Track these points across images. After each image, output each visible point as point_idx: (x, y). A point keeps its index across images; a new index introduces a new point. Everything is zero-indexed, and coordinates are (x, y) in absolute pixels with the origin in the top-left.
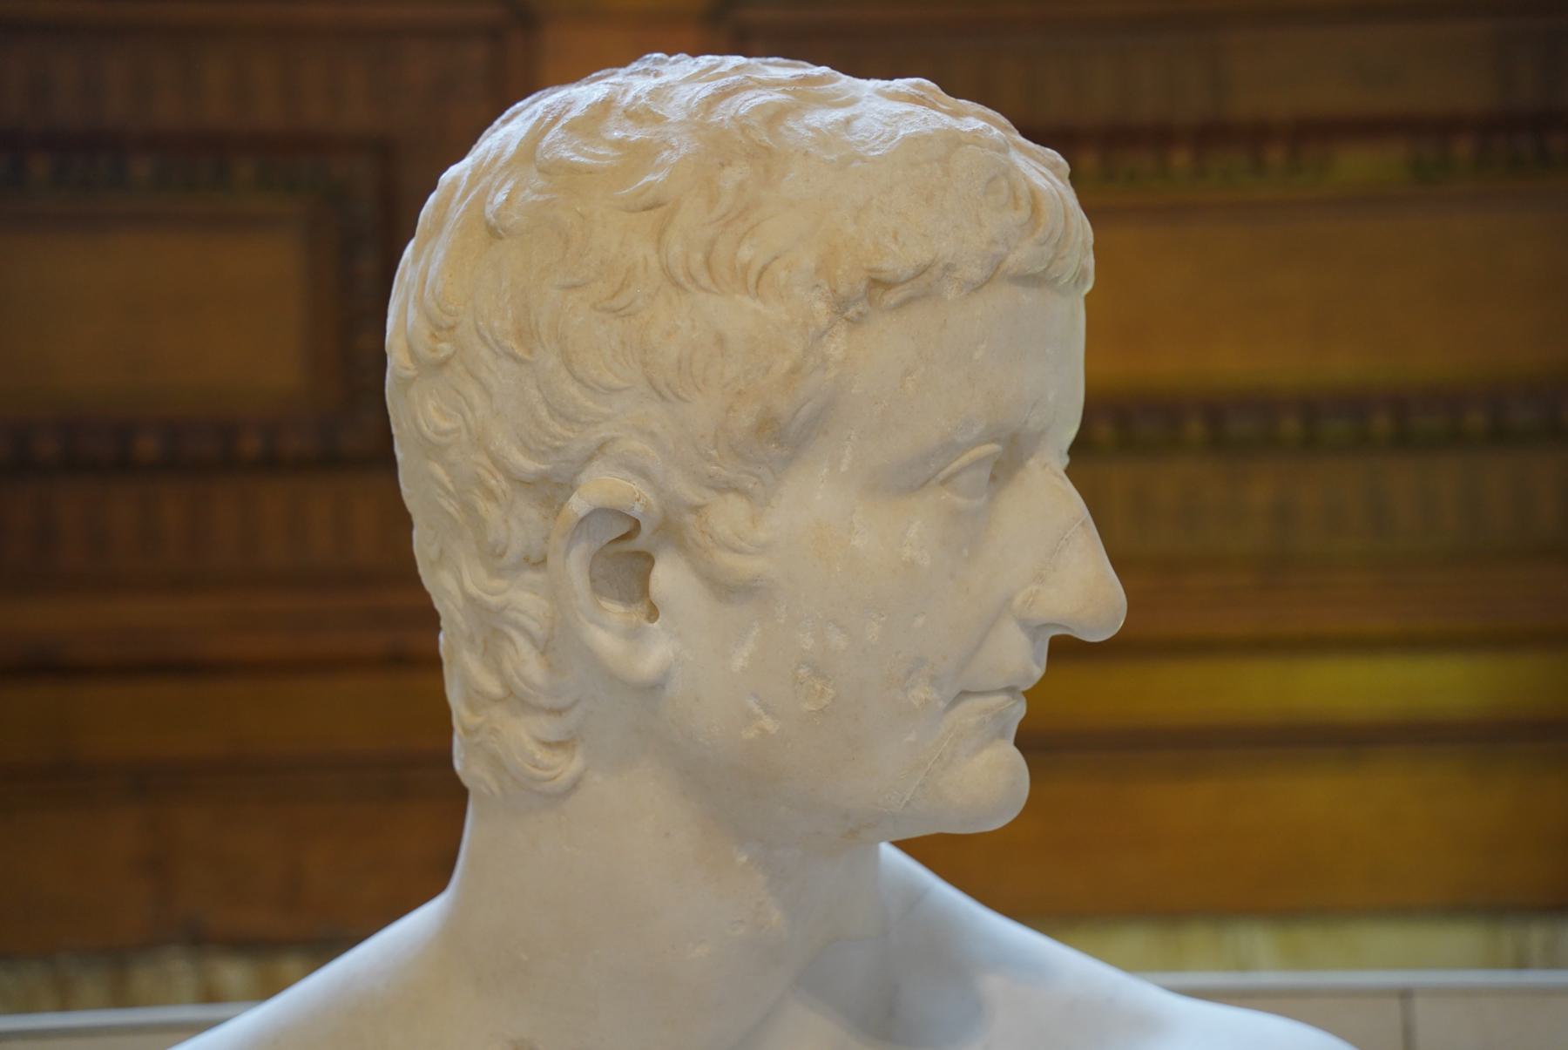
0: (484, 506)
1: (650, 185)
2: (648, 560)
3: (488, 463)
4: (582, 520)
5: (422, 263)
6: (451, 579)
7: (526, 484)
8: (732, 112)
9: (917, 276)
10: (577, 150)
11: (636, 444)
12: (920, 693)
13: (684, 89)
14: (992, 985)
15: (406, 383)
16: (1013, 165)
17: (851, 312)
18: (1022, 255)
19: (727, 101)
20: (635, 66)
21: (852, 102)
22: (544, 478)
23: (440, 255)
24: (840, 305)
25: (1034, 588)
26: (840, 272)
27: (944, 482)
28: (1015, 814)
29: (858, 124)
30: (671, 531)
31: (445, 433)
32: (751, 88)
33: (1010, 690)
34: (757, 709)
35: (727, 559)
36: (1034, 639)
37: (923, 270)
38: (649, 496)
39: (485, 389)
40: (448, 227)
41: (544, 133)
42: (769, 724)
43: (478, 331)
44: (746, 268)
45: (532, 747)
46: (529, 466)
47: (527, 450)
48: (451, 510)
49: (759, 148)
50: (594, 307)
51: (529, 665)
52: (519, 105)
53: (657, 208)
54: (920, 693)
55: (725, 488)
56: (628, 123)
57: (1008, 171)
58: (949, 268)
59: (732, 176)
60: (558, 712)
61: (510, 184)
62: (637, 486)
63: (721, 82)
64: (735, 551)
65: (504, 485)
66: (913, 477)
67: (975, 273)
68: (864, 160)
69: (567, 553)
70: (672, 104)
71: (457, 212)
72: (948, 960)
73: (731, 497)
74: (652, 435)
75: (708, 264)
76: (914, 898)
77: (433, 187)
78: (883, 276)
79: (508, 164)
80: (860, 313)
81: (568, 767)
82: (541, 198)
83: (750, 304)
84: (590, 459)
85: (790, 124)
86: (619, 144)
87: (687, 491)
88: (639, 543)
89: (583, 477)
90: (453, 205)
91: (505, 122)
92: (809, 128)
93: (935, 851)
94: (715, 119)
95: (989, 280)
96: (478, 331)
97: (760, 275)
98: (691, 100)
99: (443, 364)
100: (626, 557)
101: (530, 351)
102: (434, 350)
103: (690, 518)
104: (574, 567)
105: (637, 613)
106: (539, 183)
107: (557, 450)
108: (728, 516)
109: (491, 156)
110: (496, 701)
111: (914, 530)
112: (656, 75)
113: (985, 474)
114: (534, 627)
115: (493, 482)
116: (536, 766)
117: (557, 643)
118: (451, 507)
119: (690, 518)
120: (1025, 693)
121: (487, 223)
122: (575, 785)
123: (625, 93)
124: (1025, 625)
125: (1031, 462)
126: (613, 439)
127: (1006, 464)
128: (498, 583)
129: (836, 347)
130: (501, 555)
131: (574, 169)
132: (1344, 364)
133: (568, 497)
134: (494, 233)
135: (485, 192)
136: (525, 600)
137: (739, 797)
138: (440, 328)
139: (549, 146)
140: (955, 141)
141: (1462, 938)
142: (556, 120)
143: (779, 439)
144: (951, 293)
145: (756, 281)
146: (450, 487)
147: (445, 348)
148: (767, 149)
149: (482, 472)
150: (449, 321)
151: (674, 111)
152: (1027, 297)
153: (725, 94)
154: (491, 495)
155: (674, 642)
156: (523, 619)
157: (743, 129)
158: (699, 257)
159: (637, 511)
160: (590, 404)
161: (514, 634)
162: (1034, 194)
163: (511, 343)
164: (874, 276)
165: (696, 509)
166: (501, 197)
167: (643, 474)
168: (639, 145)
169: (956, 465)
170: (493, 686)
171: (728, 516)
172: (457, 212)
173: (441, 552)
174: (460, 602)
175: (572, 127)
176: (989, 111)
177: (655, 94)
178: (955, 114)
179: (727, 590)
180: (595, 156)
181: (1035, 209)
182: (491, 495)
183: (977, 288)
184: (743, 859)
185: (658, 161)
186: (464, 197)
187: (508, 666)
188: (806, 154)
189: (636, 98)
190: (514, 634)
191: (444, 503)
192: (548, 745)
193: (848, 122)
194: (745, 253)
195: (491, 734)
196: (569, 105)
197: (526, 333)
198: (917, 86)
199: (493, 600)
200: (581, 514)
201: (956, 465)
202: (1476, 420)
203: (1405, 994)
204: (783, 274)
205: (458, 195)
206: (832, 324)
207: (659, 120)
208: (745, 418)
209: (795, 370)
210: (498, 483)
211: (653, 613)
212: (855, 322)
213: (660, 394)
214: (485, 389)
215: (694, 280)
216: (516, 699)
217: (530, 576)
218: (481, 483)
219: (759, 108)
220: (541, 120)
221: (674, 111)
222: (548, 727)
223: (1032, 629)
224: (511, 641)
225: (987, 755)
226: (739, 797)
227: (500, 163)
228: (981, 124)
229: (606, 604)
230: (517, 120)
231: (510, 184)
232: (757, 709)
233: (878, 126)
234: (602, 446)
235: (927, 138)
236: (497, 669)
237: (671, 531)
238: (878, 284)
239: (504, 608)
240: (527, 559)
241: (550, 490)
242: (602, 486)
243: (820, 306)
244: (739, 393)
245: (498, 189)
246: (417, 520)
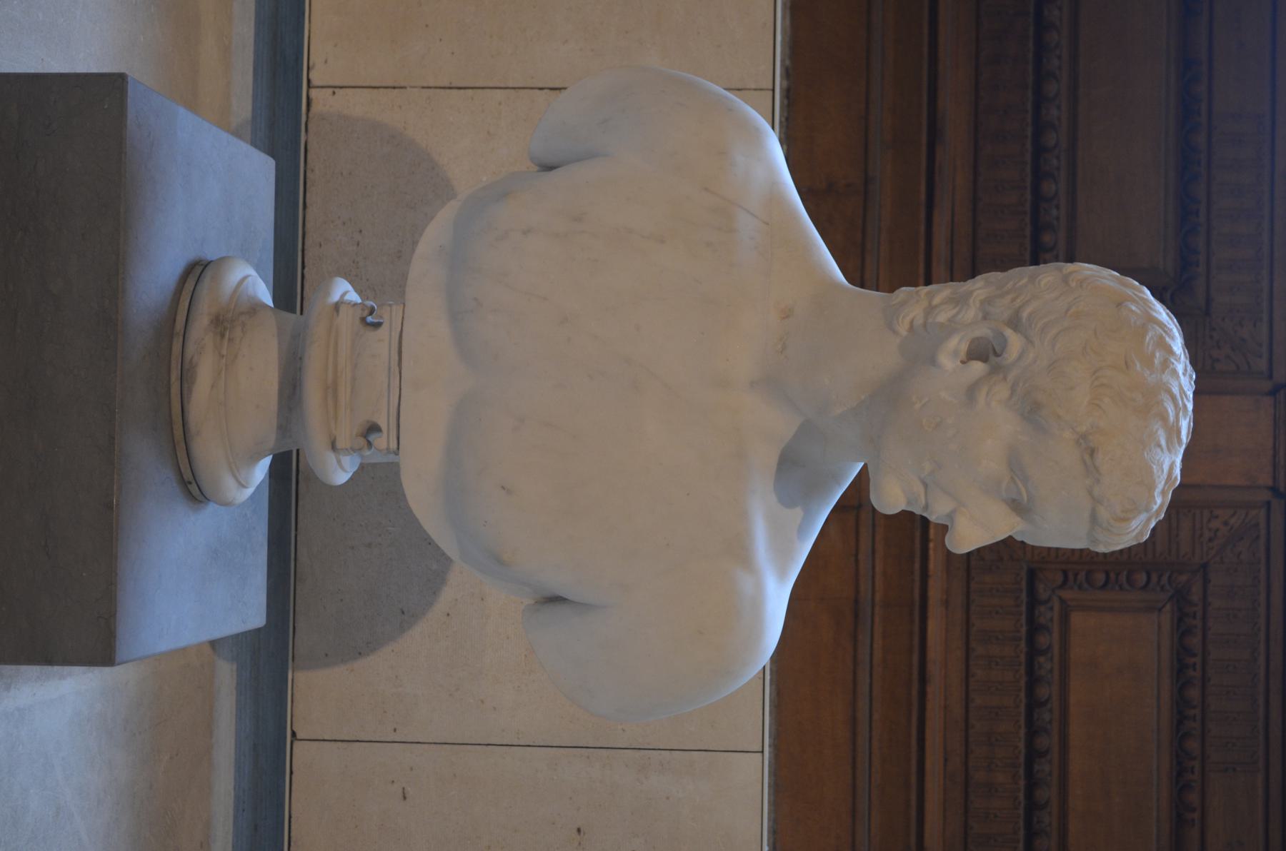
0: (1009, 297)
6: (980, 287)
7: (1017, 312)
14: (798, 513)
16: (1140, 513)
18: (1103, 513)
20: (1189, 368)
23: (1112, 284)
24: (1084, 436)
29: (1159, 450)
30: (995, 370)
33: (926, 507)
35: (985, 390)
42: (917, 406)
45: (911, 316)
46: (1025, 315)
49: (1149, 402)
55: (1013, 391)
58: (1098, 481)
66: (1014, 463)
71: (1129, 292)
76: (837, 480)
77: (1142, 283)
81: (903, 330)
84: (1026, 337)
86: (1153, 355)
87: (1011, 377)
88: (992, 358)
93: (861, 482)
100: (982, 352)
104: (983, 331)
105: (963, 355)
108: (1002, 391)
117: (949, 329)
118: (1010, 285)
122: (895, 332)
124: (954, 511)
125: (1018, 519)
127: (1018, 507)
131: (1144, 336)
134: (1119, 305)
135: (1134, 301)
136: (970, 313)
137: (888, 398)
140: (1151, 487)
143: (1031, 411)
147: (1073, 284)
151: (1166, 377)
153: (1173, 398)
154: (1013, 300)
159: (1005, 355)
165: (1005, 379)
167: (1020, 357)
169: (1020, 485)
170: (936, 301)
171: (1002, 391)
175: (1161, 339)
177: (1175, 372)
179: (971, 391)
182: (1013, 300)
183: (1090, 493)
193: (1160, 446)
195: (915, 303)
196: (1173, 338)
210: (1018, 302)
211: (963, 362)
216: (930, 310)
217: (980, 315)
221: (1166, 377)
222: (919, 321)
223: (951, 516)
228: (1159, 501)
236: (942, 304)
238: (1092, 452)
241: (1014, 323)
242: (1015, 342)
243: (1084, 429)
246: (1005, 274)
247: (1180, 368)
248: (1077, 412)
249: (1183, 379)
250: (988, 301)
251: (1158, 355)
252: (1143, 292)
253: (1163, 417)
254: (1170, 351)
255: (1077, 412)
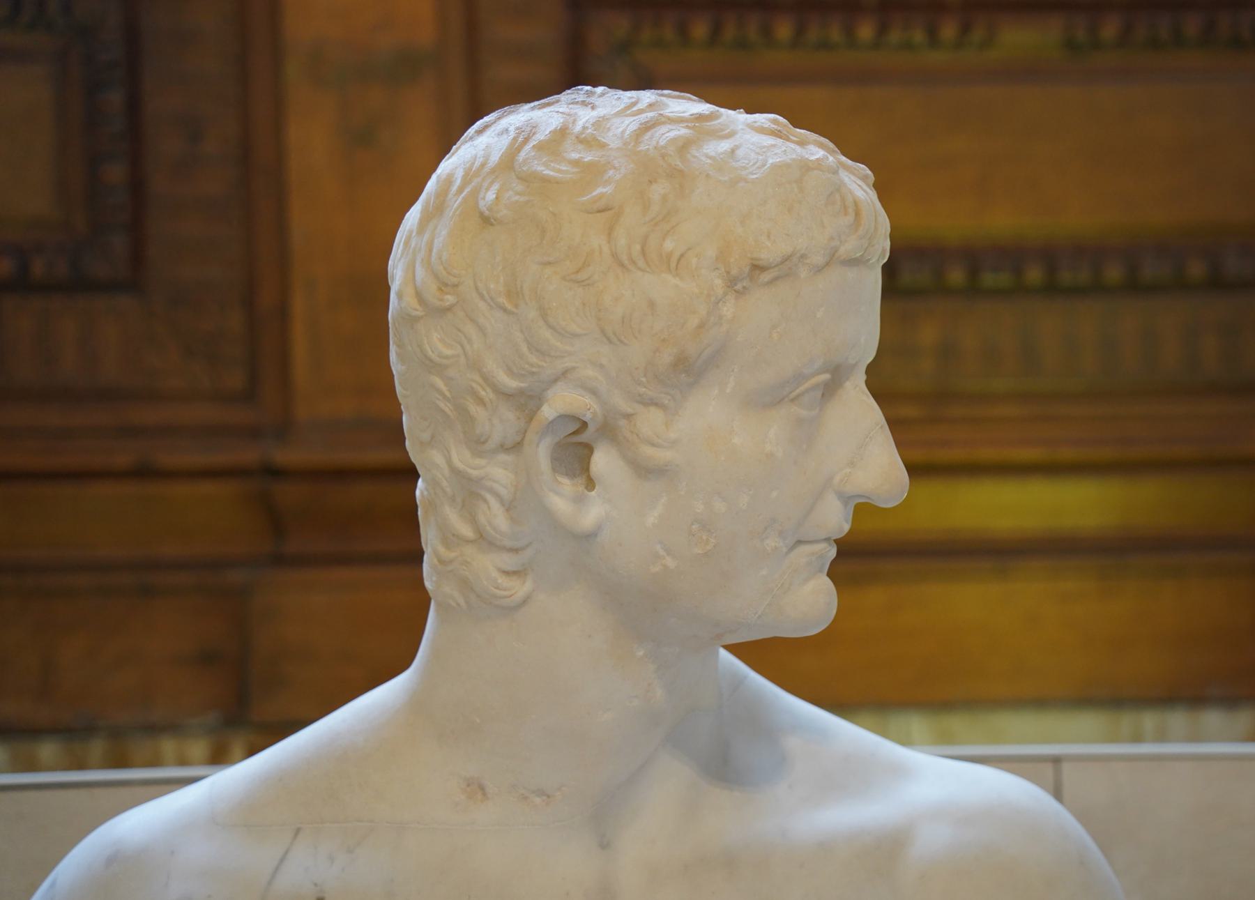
0: (473, 408)
1: (602, 195)
2: (589, 449)
3: (480, 380)
4: (552, 422)
5: (427, 236)
6: (436, 458)
8: (654, 143)
9: (782, 263)
10: (545, 165)
11: (591, 372)
12: (772, 542)
13: (617, 121)
15: (410, 320)
17: (739, 287)
18: (849, 247)
19: (649, 134)
21: (732, 134)
22: (521, 392)
24: (731, 282)
25: (848, 470)
26: (732, 260)
27: (792, 400)
28: (826, 626)
29: (740, 153)
30: (609, 431)
31: (447, 357)
32: (664, 123)
34: (662, 553)
35: (648, 451)
36: (846, 504)
37: (786, 259)
38: (596, 407)
39: (481, 330)
40: (449, 213)
41: (519, 149)
42: (670, 563)
43: (477, 289)
44: (669, 255)
45: (495, 574)
46: (512, 384)
47: (510, 372)
48: (447, 410)
49: (670, 170)
50: (564, 278)
51: (496, 518)
52: (486, 119)
53: (608, 211)
54: (772, 542)
56: (580, 147)
57: (839, 188)
58: (803, 256)
59: (659, 190)
60: (515, 550)
61: (496, 187)
62: (588, 400)
63: (644, 117)
64: (653, 445)
65: (492, 395)
67: (818, 259)
68: (746, 181)
69: (538, 446)
70: (610, 134)
71: (455, 203)
72: (763, 728)
73: (652, 409)
74: (602, 366)
75: (643, 252)
76: (738, 683)
78: (760, 263)
79: (493, 171)
80: (744, 287)
81: (521, 589)
82: (522, 199)
83: (676, 281)
84: (556, 380)
85: (694, 152)
86: (576, 163)
87: (620, 402)
88: (583, 438)
89: (550, 393)
90: (450, 196)
91: (480, 132)
92: (707, 156)
93: (766, 655)
94: (643, 147)
95: (827, 264)
96: (477, 289)
97: (679, 260)
98: (623, 132)
99: (449, 309)
100: (576, 449)
101: (516, 306)
102: (441, 300)
103: (623, 422)
104: (541, 453)
106: (520, 187)
107: (533, 373)
108: (650, 421)
109: (477, 164)
110: (468, 541)
111: (774, 432)
112: (593, 108)
113: (820, 393)
114: (503, 492)
115: (483, 393)
116: (497, 588)
118: (447, 407)
119: (623, 422)
120: (837, 541)
121: (481, 214)
122: (525, 601)
123: (574, 122)
125: (848, 384)
126: (574, 368)
127: (830, 390)
128: (478, 461)
129: (728, 310)
130: (484, 443)
131: (546, 180)
132: (1002, 221)
133: (539, 408)
134: (486, 221)
135: (475, 193)
137: (643, 612)
138: (446, 285)
139: (525, 161)
140: (806, 167)
141: (1089, 721)
142: (526, 140)
143: (687, 371)
144: (803, 273)
145: (674, 264)
146: (448, 394)
147: (450, 299)
148: (681, 171)
149: (474, 385)
150: (455, 280)
152: (851, 274)
153: (647, 127)
154: (481, 401)
155: (607, 505)
156: (495, 486)
157: (663, 156)
158: (638, 247)
159: (588, 417)
160: (558, 344)
161: (488, 496)
162: (856, 203)
163: (502, 300)
164: (756, 263)
165: (628, 416)
166: (491, 196)
167: (594, 392)
168: (591, 165)
169: (802, 388)
170: (466, 531)
171: (650, 421)
172: (455, 203)
173: (433, 437)
174: (447, 472)
175: (540, 147)
176: (822, 139)
177: (600, 123)
178: (802, 143)
179: (644, 470)
180: (560, 171)
181: (857, 214)
182: (481, 401)
183: (819, 270)
184: (641, 653)
185: (606, 177)
186: (460, 190)
187: (482, 519)
188: (708, 175)
189: (584, 128)
190: (488, 496)
191: (442, 405)
192: (507, 573)
194: (669, 245)
197: (513, 293)
198: (774, 121)
199: (474, 473)
200: (551, 419)
201: (802, 388)
202: (1114, 273)
203: (1056, 760)
204: (694, 260)
205: (454, 188)
206: (725, 294)
207: (603, 146)
208: (667, 357)
209: (701, 326)
210: (487, 394)
211: (590, 484)
212: (739, 294)
213: (608, 339)
214: (481, 330)
215: (634, 262)
216: (484, 540)
217: (503, 457)
218: (474, 394)
219: (674, 140)
220: (515, 139)
222: (509, 561)
223: (845, 498)
224: (485, 501)
225: (811, 586)
226: (643, 612)
227: (486, 170)
228: (820, 153)
229: (560, 479)
230: (488, 133)
231: (496, 187)
232: (662, 553)
233: (753, 155)
234: (565, 373)
235: (788, 166)
236: (473, 521)
237: (609, 431)
238: (757, 268)
239: (482, 478)
240: (502, 446)
241: (527, 402)
242: (561, 401)
243: (718, 282)
244: (664, 340)
245: (488, 189)
247: (585, 117)
248: (640, 293)
249: (601, 113)
250: (477, 444)
251: (575, 156)
252: (449, 180)
253: (684, 146)
254: (561, 133)
255: (640, 293)
